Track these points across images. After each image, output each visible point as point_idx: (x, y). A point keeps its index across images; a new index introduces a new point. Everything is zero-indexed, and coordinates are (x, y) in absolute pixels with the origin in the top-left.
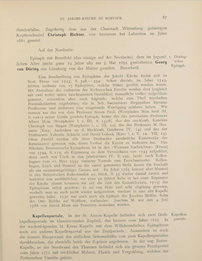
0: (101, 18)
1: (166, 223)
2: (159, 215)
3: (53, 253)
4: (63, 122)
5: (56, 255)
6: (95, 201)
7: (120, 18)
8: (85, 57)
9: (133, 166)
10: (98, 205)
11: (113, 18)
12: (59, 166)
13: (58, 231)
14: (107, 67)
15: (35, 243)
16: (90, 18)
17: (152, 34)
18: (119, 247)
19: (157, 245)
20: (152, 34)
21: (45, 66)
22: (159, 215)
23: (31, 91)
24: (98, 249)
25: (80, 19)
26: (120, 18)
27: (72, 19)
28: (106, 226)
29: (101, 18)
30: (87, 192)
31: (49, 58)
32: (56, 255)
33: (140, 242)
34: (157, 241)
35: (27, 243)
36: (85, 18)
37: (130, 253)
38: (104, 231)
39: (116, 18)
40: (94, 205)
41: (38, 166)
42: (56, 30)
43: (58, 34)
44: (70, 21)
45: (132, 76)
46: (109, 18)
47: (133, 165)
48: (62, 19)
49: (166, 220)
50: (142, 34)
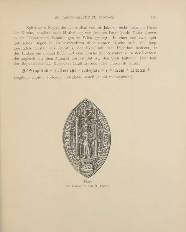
0: (94, 17)
1: (155, 51)
2: (36, 49)
3: (39, 59)
4: (87, 64)
5: (41, 61)
6: (150, 58)
7: (113, 18)
8: (121, 37)
9: (110, 60)
10: (88, 28)
11: (106, 17)
12: (73, 53)
13: (30, 38)
14: (80, 27)
15: (109, 17)
16: (84, 17)
17: (143, 28)
18: (42, 38)
19: (67, 62)
20: (143, 28)
21: (139, 51)
22: (36, 49)
23: (66, 33)
24: (54, 60)
25: (75, 18)
26: (113, 18)
27: (66, 18)
28: (15, 33)
29: (94, 17)
30: (141, 48)
31: (101, 53)
32: (41, 61)
33: (107, 48)
34: (37, 43)
35: (28, 33)
36: (79, 17)
37: (16, 44)
38: (81, 33)
39: (109, 17)
40: (48, 33)
41: (155, 53)
42: (136, 28)
43: (16, 54)
44: (64, 19)
45: (27, 33)
46: (102, 17)
47: (110, 58)
48: (57, 18)
49: (114, 38)
50: (89, 59)
